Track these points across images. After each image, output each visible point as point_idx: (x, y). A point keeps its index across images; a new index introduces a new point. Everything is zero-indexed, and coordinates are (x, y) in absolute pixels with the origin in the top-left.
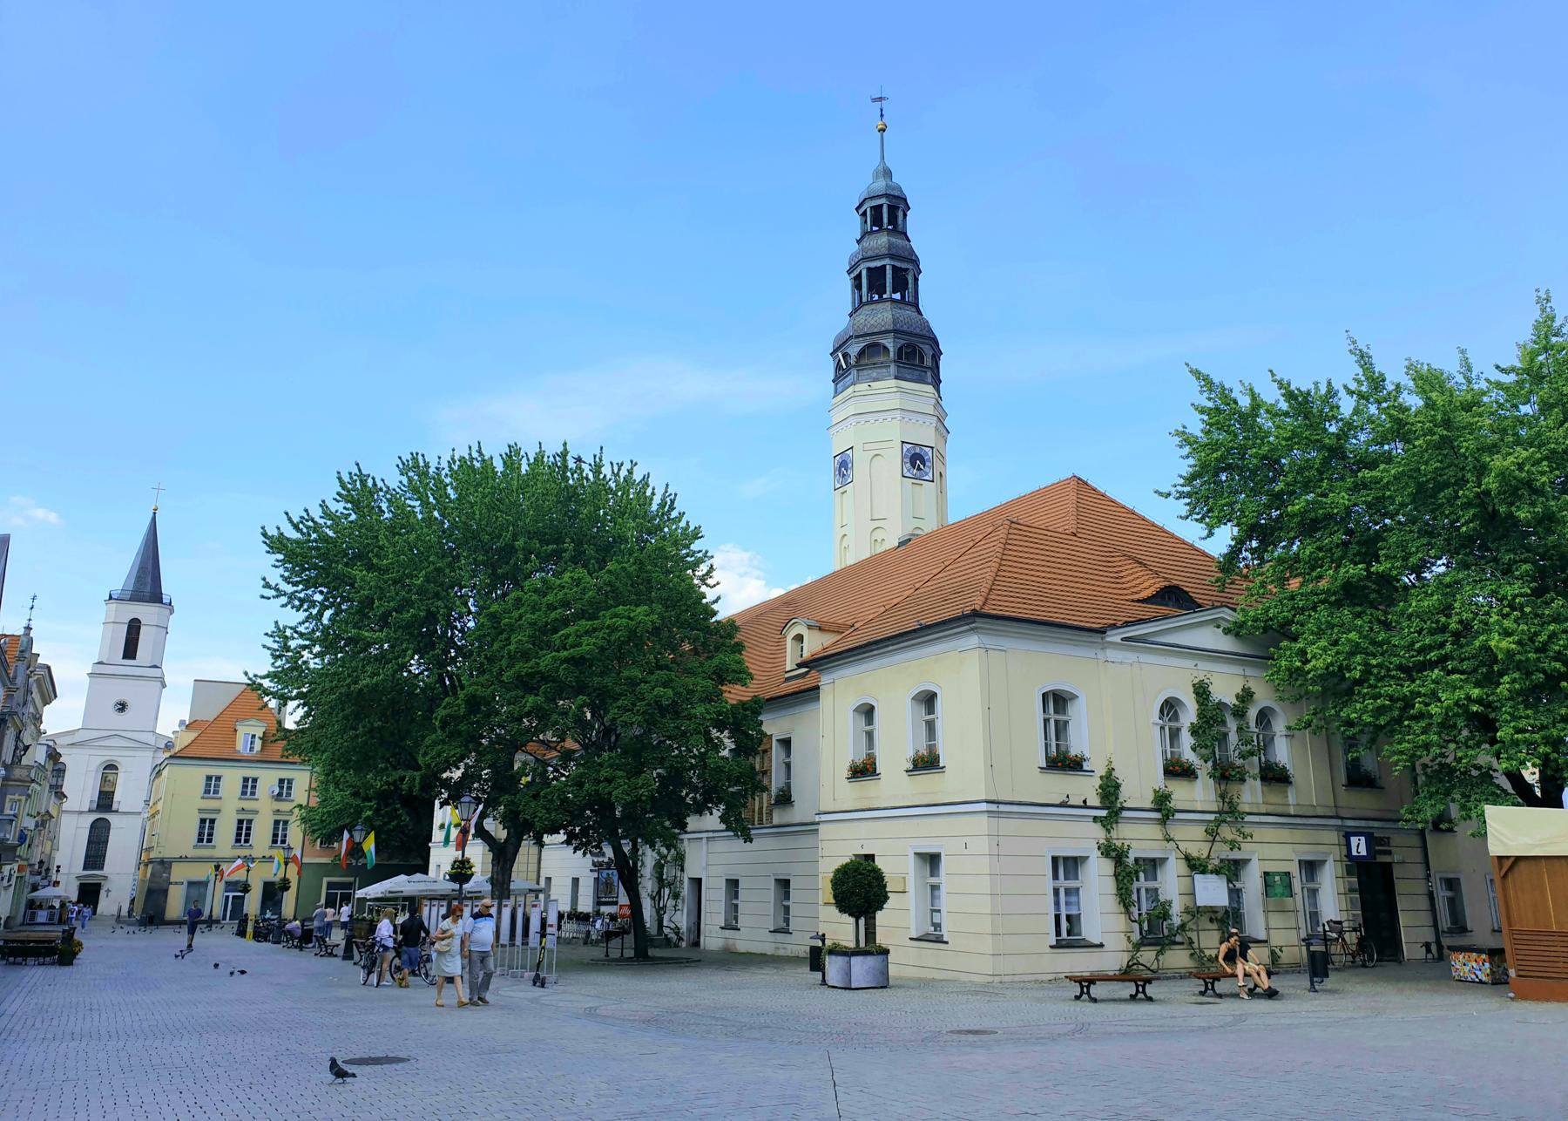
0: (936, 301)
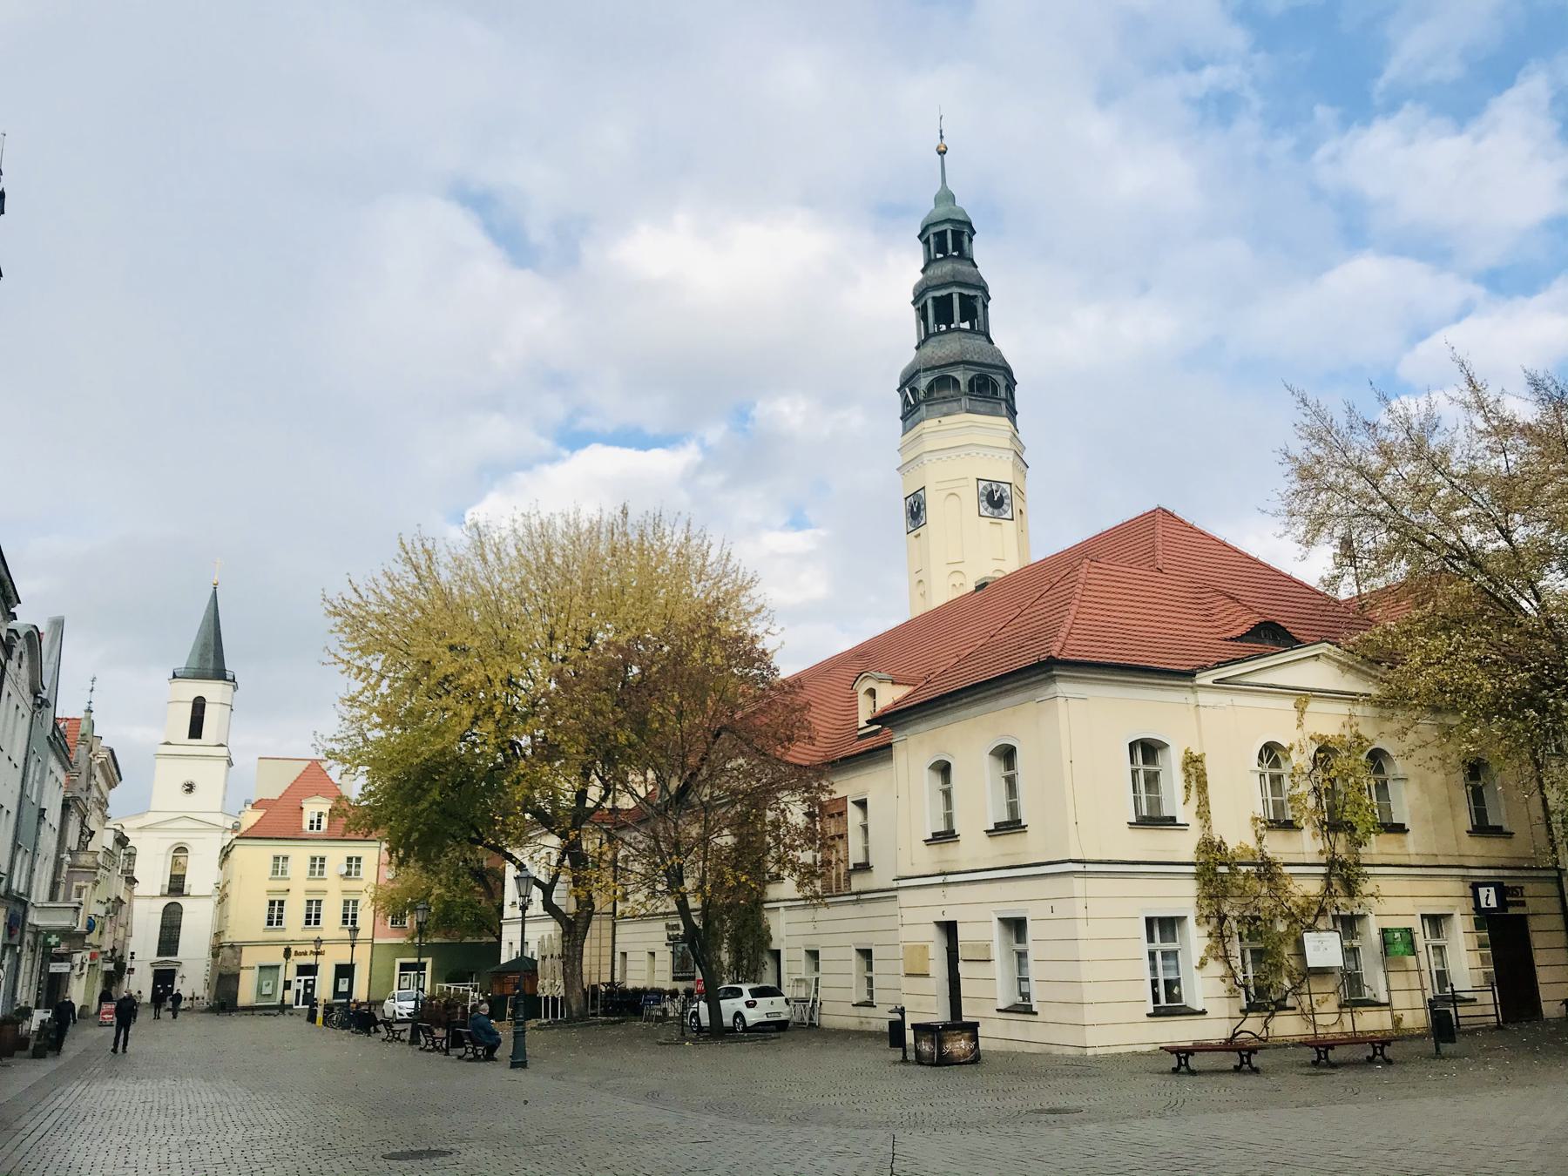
0: (1011, 333)
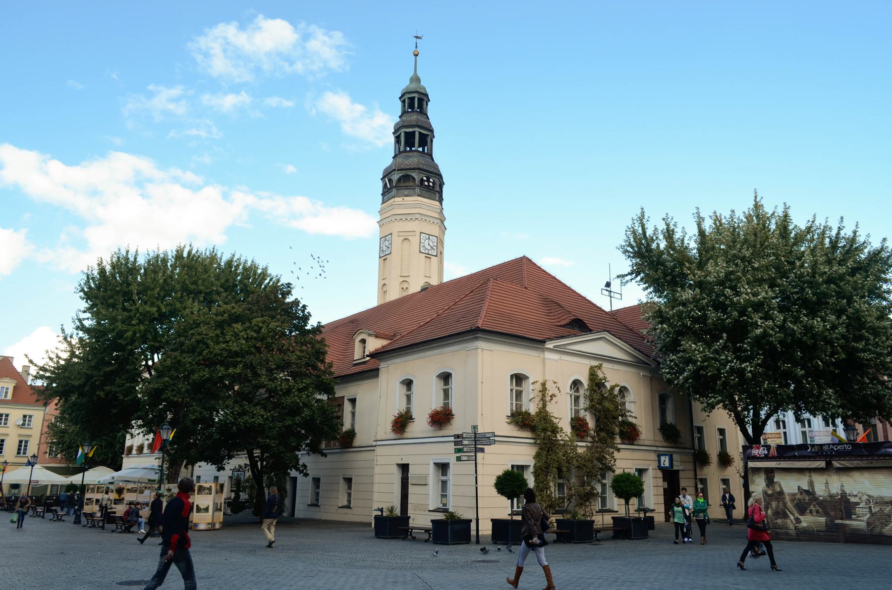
0: (443, 153)
